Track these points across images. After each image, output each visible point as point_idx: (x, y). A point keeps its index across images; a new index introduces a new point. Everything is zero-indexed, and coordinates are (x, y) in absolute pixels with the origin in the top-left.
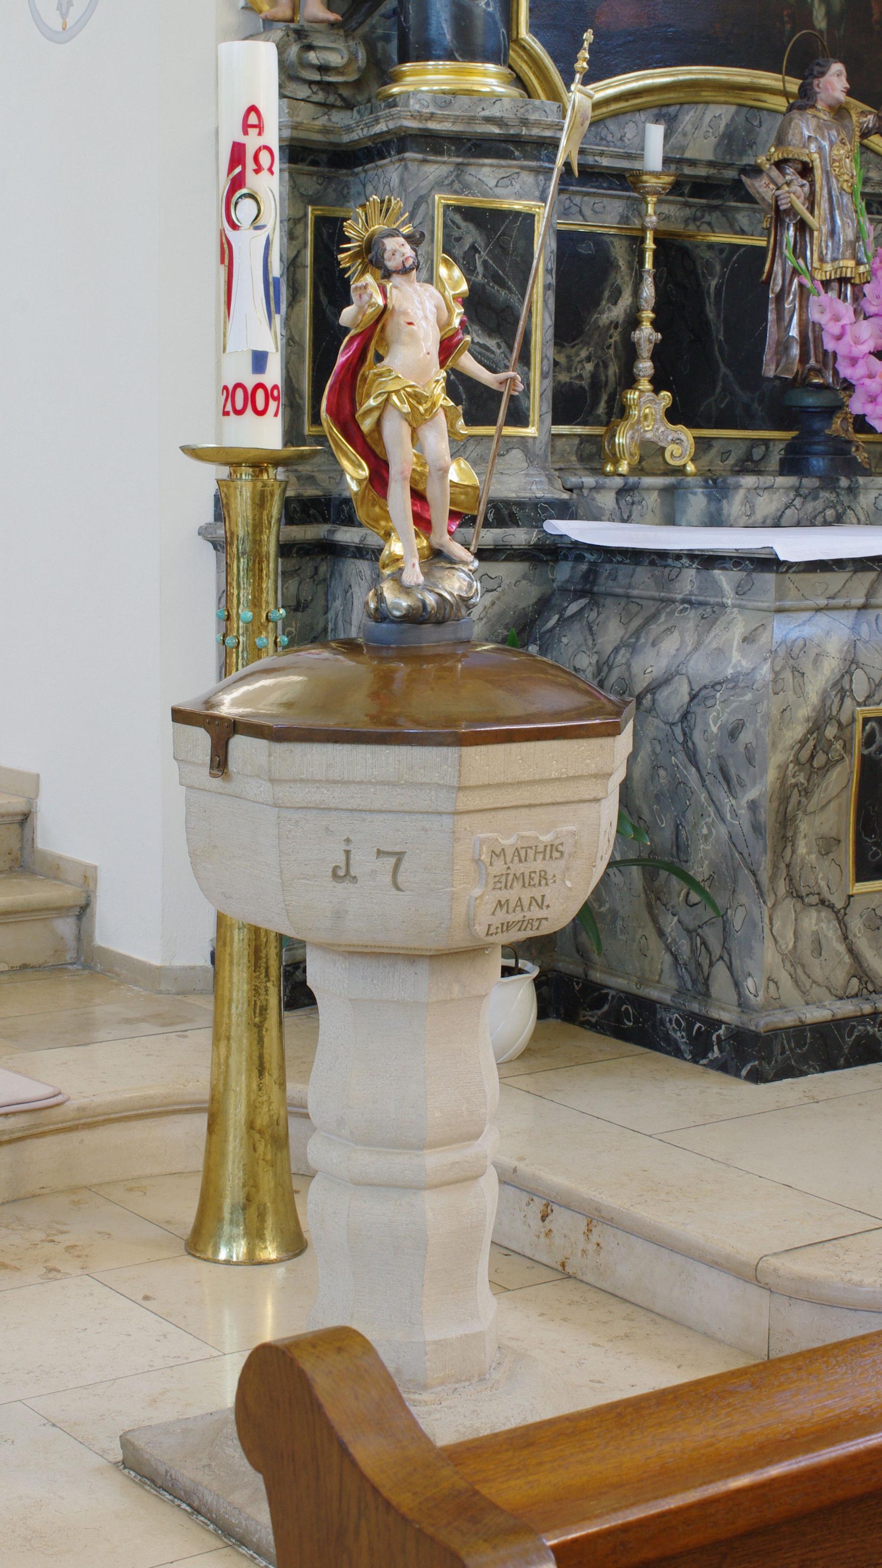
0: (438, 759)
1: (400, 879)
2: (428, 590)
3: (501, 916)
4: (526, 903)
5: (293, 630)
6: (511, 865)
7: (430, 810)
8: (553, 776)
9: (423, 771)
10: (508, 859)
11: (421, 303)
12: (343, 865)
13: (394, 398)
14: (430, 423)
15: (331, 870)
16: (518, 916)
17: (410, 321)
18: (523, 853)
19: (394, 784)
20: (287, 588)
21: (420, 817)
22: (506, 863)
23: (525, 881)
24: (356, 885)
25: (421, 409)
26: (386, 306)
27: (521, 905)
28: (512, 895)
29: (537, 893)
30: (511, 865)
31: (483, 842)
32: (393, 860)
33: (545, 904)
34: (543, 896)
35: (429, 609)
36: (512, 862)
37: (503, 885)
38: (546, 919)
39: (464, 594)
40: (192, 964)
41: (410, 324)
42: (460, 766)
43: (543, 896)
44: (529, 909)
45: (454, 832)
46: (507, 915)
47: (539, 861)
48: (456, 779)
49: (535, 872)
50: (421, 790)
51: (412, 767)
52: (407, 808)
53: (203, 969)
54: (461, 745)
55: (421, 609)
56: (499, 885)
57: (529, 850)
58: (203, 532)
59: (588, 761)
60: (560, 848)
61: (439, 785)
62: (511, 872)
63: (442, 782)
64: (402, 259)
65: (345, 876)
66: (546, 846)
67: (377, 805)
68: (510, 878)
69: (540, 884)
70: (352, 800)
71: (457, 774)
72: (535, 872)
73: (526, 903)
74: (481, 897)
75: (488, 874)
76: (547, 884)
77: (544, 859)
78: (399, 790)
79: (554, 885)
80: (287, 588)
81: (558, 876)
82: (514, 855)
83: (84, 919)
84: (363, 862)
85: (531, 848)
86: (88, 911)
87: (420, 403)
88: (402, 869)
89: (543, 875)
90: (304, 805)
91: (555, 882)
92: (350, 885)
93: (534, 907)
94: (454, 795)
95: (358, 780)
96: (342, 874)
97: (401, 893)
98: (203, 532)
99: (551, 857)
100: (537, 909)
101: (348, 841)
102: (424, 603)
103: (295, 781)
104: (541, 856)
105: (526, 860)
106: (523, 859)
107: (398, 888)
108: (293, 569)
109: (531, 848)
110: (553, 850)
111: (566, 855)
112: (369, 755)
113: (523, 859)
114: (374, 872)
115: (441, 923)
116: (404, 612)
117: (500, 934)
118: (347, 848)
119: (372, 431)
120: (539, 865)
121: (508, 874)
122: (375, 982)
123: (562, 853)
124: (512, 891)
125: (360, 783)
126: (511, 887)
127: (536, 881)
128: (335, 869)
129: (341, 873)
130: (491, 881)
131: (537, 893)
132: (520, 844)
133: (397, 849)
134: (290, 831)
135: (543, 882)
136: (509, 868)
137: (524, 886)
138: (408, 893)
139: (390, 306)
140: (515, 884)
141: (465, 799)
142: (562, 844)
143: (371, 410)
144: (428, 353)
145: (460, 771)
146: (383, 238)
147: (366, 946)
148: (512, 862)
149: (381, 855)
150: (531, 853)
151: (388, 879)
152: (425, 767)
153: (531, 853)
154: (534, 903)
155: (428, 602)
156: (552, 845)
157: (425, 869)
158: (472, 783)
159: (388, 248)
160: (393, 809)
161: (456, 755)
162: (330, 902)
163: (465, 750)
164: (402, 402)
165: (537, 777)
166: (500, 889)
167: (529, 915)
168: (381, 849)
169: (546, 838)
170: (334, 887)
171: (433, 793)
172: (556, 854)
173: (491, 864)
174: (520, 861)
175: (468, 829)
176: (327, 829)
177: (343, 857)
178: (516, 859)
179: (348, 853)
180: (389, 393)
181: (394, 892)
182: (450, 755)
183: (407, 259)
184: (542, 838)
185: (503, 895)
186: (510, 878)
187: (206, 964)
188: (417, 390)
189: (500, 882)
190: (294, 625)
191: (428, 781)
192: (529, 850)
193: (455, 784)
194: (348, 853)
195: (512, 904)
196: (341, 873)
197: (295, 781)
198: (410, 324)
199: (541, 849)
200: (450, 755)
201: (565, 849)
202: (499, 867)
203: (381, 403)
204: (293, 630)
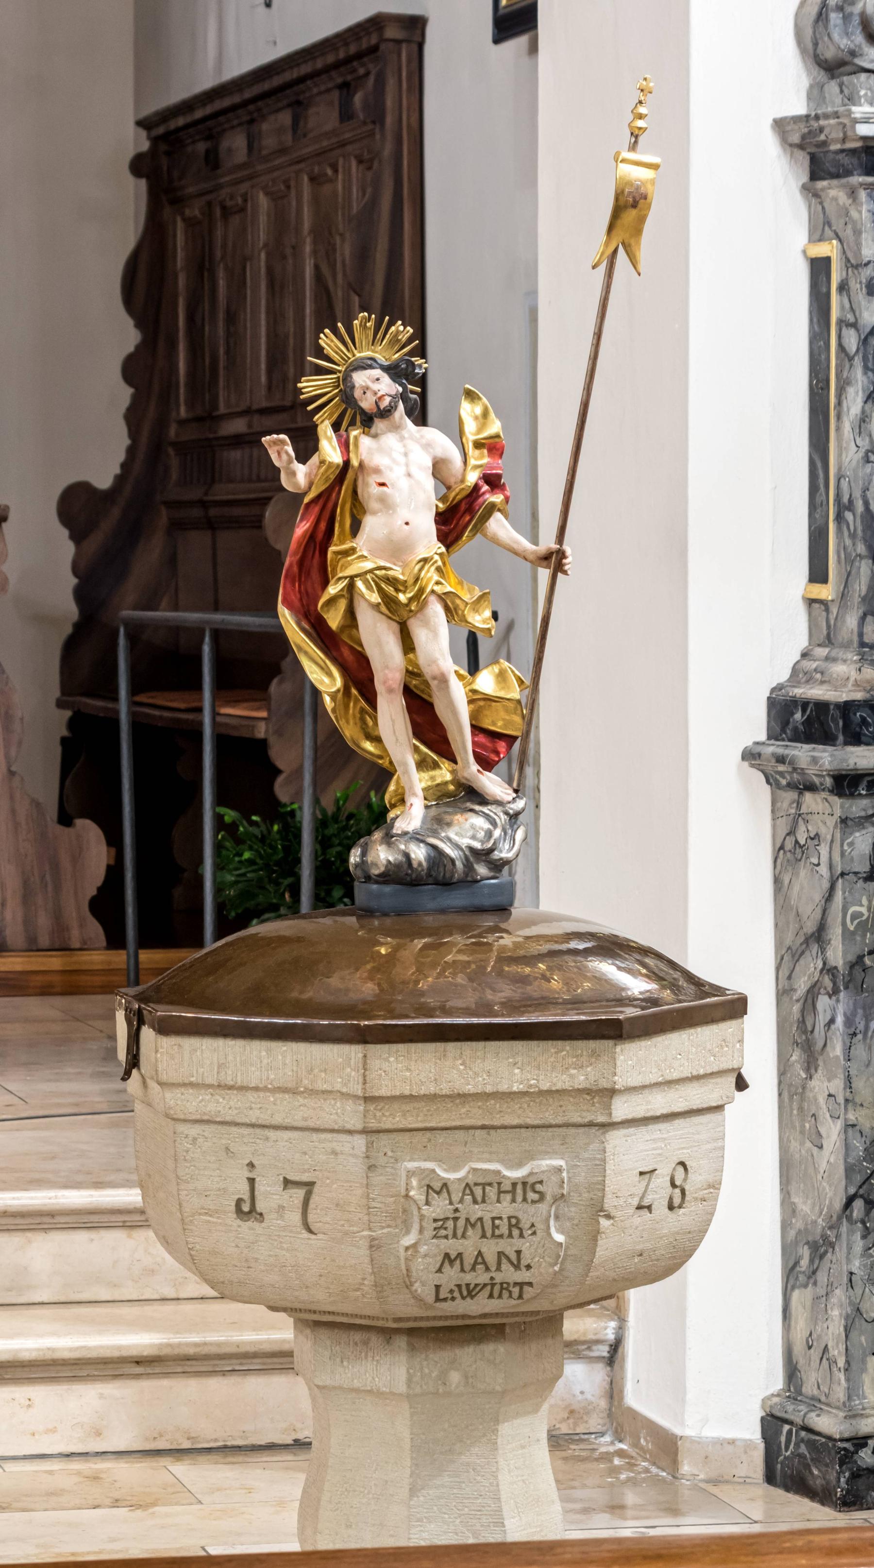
0: (341, 1060)
1: (311, 1218)
3: (451, 1276)
4: (491, 1259)
5: (864, 910)
6: (459, 1206)
7: (336, 1127)
8: (515, 1089)
9: (323, 1075)
10: (456, 1198)
12: (246, 1197)
13: (360, 584)
14: (418, 615)
15: (233, 1204)
16: (482, 1277)
17: (381, 481)
18: (478, 1191)
19: (294, 1092)
20: (851, 844)
21: (329, 1136)
22: (451, 1203)
23: (489, 1230)
24: (263, 1225)
25: (403, 598)
26: (347, 463)
27: (484, 1262)
28: (469, 1246)
29: (505, 1246)
30: (459, 1206)
31: (410, 1174)
32: (300, 1193)
33: (524, 1262)
34: (519, 1252)
35: (415, 865)
36: (461, 1201)
37: (450, 1232)
38: (530, 1284)
39: (477, 845)
40: (730, 1435)
41: (383, 484)
42: (365, 1069)
43: (519, 1252)
44: (499, 1269)
45: (367, 1157)
46: (462, 1275)
47: (505, 1204)
48: (360, 1087)
49: (500, 1218)
50: (325, 1100)
51: (312, 1070)
52: (311, 1124)
53: (748, 1445)
54: (365, 1042)
55: (405, 866)
56: (443, 1232)
57: (488, 1188)
58: (750, 756)
60: (538, 1187)
61: (342, 1094)
62: (462, 1216)
63: (344, 1090)
64: (374, 398)
65: (250, 1212)
66: (514, 1185)
67: (278, 1120)
68: (461, 1223)
69: (510, 1236)
70: (251, 1112)
71: (361, 1080)
72: (500, 1218)
73: (491, 1259)
74: (415, 1246)
75: (422, 1217)
76: (521, 1236)
77: (514, 1200)
78: (301, 1100)
79: (534, 1238)
80: (851, 844)
81: (540, 1226)
82: (464, 1194)
83: (616, 1366)
84: (270, 1195)
85: (490, 1184)
86: (620, 1350)
87: (397, 590)
88: (312, 1205)
89: (514, 1224)
90: (198, 1117)
91: (534, 1233)
92: (256, 1225)
93: (505, 1265)
94: (362, 1108)
95: (253, 1085)
96: (247, 1210)
97: (313, 1237)
98: (750, 756)
99: (525, 1199)
100: (512, 1269)
101: (251, 1165)
102: (407, 856)
103: (184, 1085)
104: (509, 1197)
105: (484, 1201)
106: (479, 1199)
107: (310, 1231)
108: (863, 814)
109: (490, 1184)
110: (528, 1188)
111: (549, 1198)
112: (264, 1053)
113: (479, 1199)
114: (281, 1208)
115: (364, 1279)
116: (382, 869)
117: (459, 1300)
118: (251, 1176)
119: (343, 628)
120: (505, 1208)
121: (456, 1219)
122: (345, 1363)
123: (542, 1196)
124: (466, 1242)
125: (256, 1089)
126: (464, 1236)
127: (504, 1230)
128: (239, 1202)
129: (246, 1208)
130: (430, 1226)
131: (509, 1247)
132: (471, 1179)
133: (305, 1178)
134: (187, 1151)
135: (516, 1232)
136: (456, 1210)
137: (484, 1236)
138: (320, 1236)
139: (355, 463)
140: (470, 1232)
141: (378, 1114)
142: (541, 1182)
143: (332, 601)
144: (407, 524)
145: (364, 1076)
147: (315, 1312)
148: (461, 1201)
149: (290, 1186)
150: (492, 1192)
151: (296, 1217)
153: (492, 1192)
154: (504, 1260)
155: (413, 856)
156: (524, 1184)
157: (337, 1205)
158: (384, 1092)
159: (357, 385)
160: (296, 1124)
161: (360, 1055)
162: (237, 1246)
163: (372, 1048)
165: (489, 1089)
166: (446, 1237)
167: (499, 1277)
168: (288, 1177)
169: (517, 1174)
170: (239, 1226)
171: (338, 1104)
172: (532, 1196)
173: (427, 1203)
174: (475, 1202)
175: (390, 1154)
176: (227, 1149)
177: (246, 1187)
178: (468, 1198)
179: (252, 1181)
180: (352, 578)
181: (305, 1235)
182: (353, 1054)
183: (381, 398)
184: (507, 1173)
185: (453, 1246)
186: (461, 1223)
187: (752, 1437)
188: (390, 573)
189: (446, 1229)
190: (865, 901)
191: (329, 1088)
192: (488, 1188)
193: (360, 1093)
194: (252, 1181)
195: (469, 1260)
196: (246, 1208)
197: (184, 1085)
198: (383, 484)
199: (507, 1186)
200: (353, 1054)
201: (549, 1189)
202: (440, 1207)
203: (342, 590)
204: (864, 910)
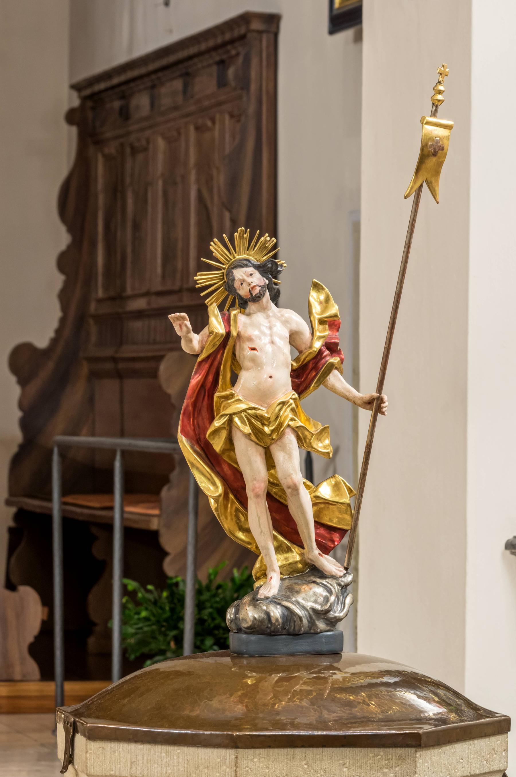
0: (219, 760)
2: (275, 603)
9: (206, 771)
11: (270, 328)
13: (236, 420)
17: (253, 346)
25: (267, 430)
26: (228, 334)
35: (273, 621)
39: (318, 607)
41: (254, 349)
42: (237, 767)
51: (198, 767)
55: (267, 621)
59: (386, 770)
87: (263, 424)
102: (268, 614)
112: (164, 755)
119: (224, 451)
139: (234, 333)
143: (217, 431)
144: (271, 377)
146: (233, 268)
152: (208, 767)
155: (272, 614)
159: (236, 278)
161: (233, 757)
164: (243, 422)
180: (231, 415)
182: (228, 756)
183: (253, 288)
198: (254, 349)
200: (228, 756)
203: (224, 424)
